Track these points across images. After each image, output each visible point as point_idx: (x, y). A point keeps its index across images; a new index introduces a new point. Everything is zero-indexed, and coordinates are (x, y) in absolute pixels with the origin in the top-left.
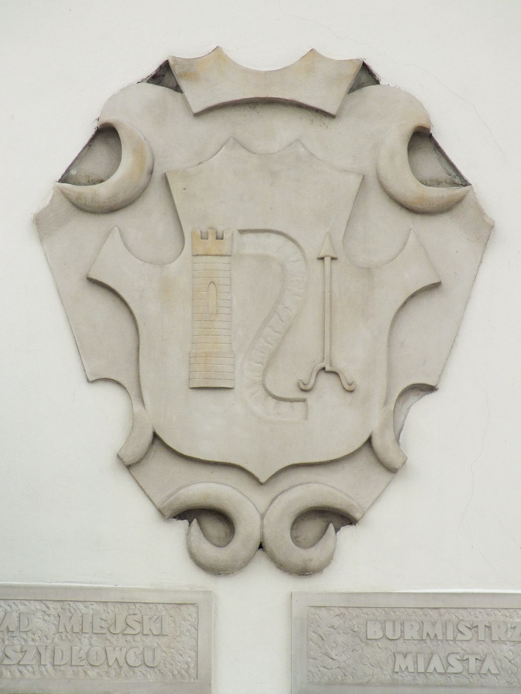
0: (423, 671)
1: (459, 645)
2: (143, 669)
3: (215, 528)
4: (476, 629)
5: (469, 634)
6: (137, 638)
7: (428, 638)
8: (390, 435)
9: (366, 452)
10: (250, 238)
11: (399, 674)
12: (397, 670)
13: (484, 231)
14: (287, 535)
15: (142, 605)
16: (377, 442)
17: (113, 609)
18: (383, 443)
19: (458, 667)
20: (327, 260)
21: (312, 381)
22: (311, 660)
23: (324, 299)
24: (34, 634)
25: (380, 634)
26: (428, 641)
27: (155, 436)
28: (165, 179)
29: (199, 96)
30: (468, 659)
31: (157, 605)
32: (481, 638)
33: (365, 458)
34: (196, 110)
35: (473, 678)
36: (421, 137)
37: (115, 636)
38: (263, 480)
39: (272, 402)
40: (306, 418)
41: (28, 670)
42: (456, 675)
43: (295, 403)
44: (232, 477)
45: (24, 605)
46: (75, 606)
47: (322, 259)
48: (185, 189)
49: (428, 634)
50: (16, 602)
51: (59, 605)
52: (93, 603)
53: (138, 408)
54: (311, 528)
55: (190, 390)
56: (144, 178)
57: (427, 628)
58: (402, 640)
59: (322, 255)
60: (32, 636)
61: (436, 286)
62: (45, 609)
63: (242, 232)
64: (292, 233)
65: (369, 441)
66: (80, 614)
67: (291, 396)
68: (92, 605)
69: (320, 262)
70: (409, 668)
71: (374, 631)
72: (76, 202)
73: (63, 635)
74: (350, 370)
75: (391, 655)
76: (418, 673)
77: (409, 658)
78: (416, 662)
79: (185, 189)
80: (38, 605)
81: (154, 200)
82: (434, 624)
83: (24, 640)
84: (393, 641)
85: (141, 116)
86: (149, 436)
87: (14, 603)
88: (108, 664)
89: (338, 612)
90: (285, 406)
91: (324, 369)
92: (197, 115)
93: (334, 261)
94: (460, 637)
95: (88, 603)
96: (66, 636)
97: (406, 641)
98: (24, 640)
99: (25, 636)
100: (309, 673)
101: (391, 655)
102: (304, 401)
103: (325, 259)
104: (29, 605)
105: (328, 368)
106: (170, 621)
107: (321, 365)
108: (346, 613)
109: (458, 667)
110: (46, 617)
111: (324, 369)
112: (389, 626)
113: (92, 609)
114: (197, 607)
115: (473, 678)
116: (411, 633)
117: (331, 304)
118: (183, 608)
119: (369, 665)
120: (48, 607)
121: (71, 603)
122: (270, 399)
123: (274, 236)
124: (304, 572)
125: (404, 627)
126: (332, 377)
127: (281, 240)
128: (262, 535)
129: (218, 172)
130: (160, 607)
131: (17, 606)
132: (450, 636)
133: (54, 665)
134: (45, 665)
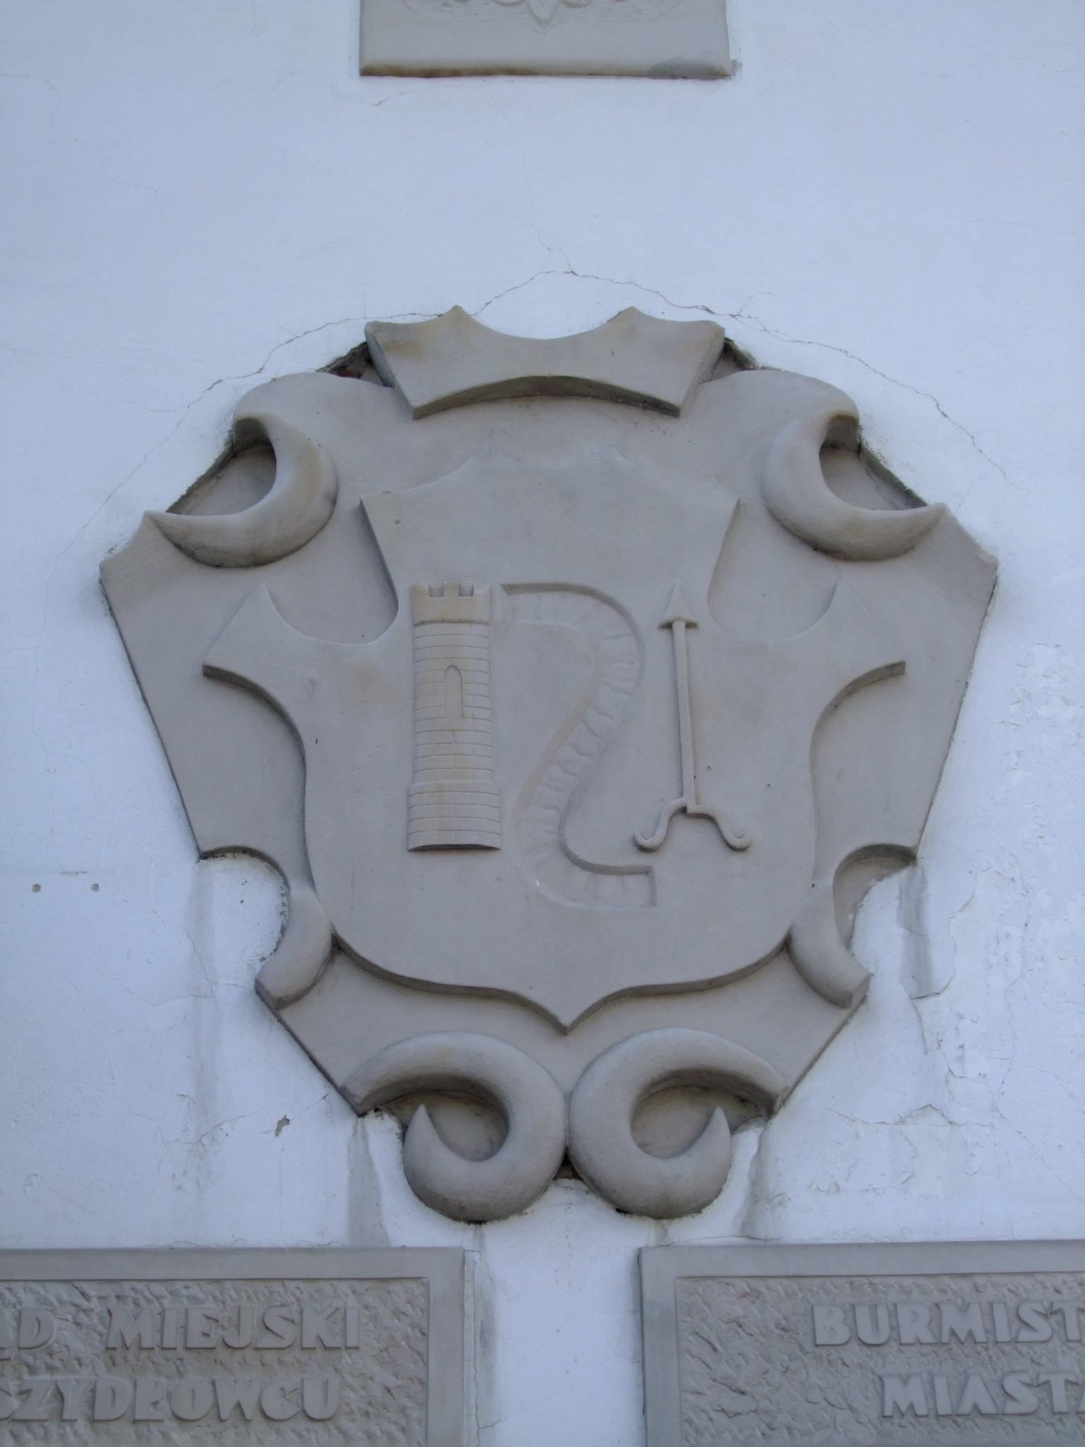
0: (949, 1412)
1: (1024, 1352)
2: (302, 1424)
3: (465, 1125)
4: (1059, 1317)
5: (1044, 1329)
6: (288, 1357)
7: (953, 1339)
8: (830, 936)
9: (783, 966)
10: (524, 600)
11: (896, 1421)
12: (888, 1412)
13: (976, 579)
14: (624, 1126)
15: (301, 1284)
16: (804, 945)
17: (234, 1295)
18: (820, 946)
19: (1029, 1400)
20: (679, 628)
21: (661, 832)
22: (691, 1398)
23: (676, 693)
24: (51, 1355)
25: (843, 1335)
26: (954, 1346)
27: (338, 946)
28: (362, 514)
29: (420, 384)
30: (1048, 1382)
31: (335, 1283)
32: (1073, 1334)
33: (780, 980)
34: (418, 401)
35: (1063, 1423)
36: (842, 441)
37: (238, 1353)
38: (566, 1020)
39: (582, 876)
40: (653, 903)
41: (34, 1435)
42: (1026, 1419)
43: (627, 877)
44: (501, 1019)
45: (32, 1291)
46: (147, 1293)
47: (669, 626)
48: (398, 522)
49: (953, 1332)
50: (13, 1285)
51: (110, 1291)
52: (189, 1283)
53: (299, 891)
54: (677, 1117)
55: (411, 855)
56: (319, 507)
57: (951, 1318)
58: (894, 1344)
59: (668, 616)
60: (48, 1359)
61: (894, 671)
62: (80, 1300)
63: (511, 589)
64: (609, 590)
65: (786, 946)
66: (159, 1309)
67: (621, 862)
68: (187, 1288)
69: (666, 632)
70: (916, 1406)
71: (830, 1326)
72: (182, 543)
73: (118, 1356)
74: (736, 822)
75: (873, 1381)
76: (938, 1416)
77: (915, 1383)
78: (932, 1394)
79: (398, 522)
80: (64, 1292)
81: (338, 548)
82: (964, 1308)
83: (28, 1366)
84: (874, 1349)
85: (318, 428)
86: (323, 943)
87: (9, 1289)
88: (219, 1416)
89: (743, 1286)
90: (608, 884)
91: (684, 810)
92: (423, 413)
93: (691, 631)
94: (1025, 1335)
95: (178, 1286)
96: (364, 1388)
97: (903, 1348)
98: (28, 1366)
99: (31, 1360)
100: (687, 1425)
101: (873, 1381)
102: (647, 872)
103: (674, 625)
104: (43, 1292)
105: (692, 808)
106: (364, 1320)
107: (675, 803)
108: (763, 1290)
109: (1029, 1400)
110: (83, 1318)
111: (684, 810)
112: (863, 1314)
113: (188, 1298)
114: (427, 1286)
115: (1063, 1423)
116: (915, 1327)
117: (691, 703)
118: (394, 1287)
119: (824, 1404)
120: (83, 1294)
121: (139, 1286)
122: (577, 869)
123: (572, 600)
124: (665, 1210)
125: (897, 1319)
126: (704, 828)
127: (588, 603)
128: (569, 1130)
129: (463, 505)
130: (344, 1287)
131: (15, 1295)
132: (1003, 1335)
133: (92, 1421)
134: (72, 1421)
